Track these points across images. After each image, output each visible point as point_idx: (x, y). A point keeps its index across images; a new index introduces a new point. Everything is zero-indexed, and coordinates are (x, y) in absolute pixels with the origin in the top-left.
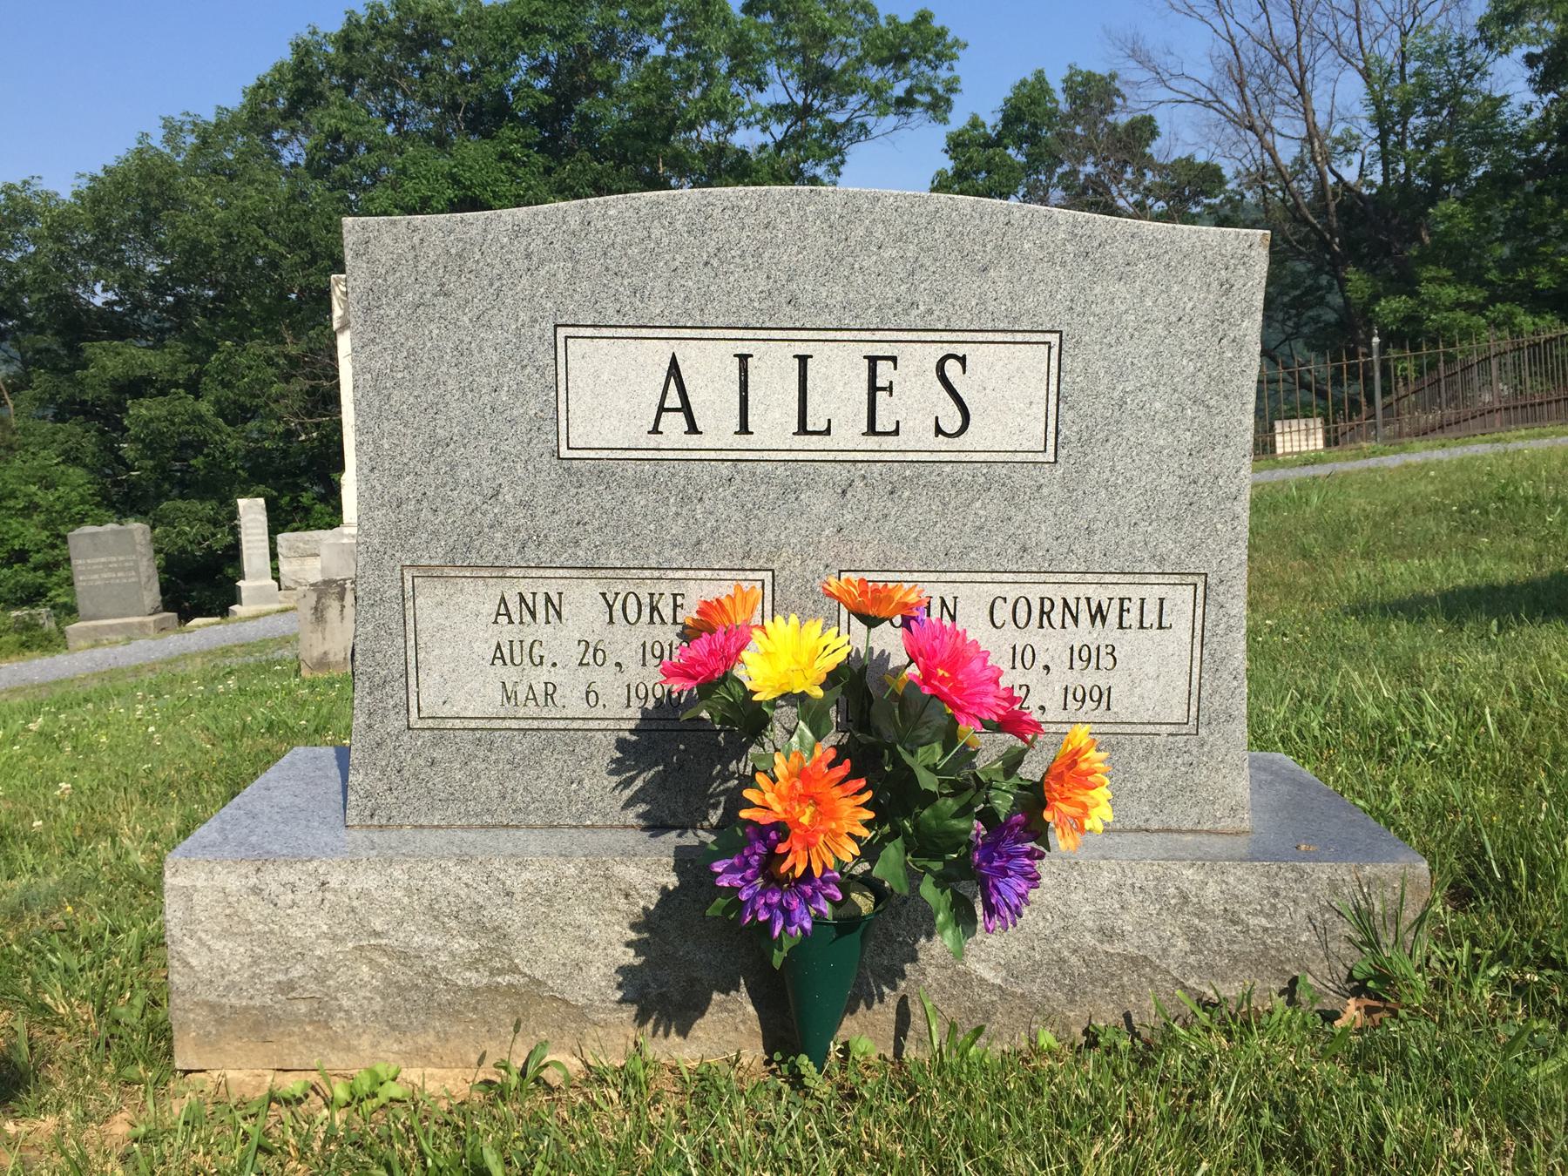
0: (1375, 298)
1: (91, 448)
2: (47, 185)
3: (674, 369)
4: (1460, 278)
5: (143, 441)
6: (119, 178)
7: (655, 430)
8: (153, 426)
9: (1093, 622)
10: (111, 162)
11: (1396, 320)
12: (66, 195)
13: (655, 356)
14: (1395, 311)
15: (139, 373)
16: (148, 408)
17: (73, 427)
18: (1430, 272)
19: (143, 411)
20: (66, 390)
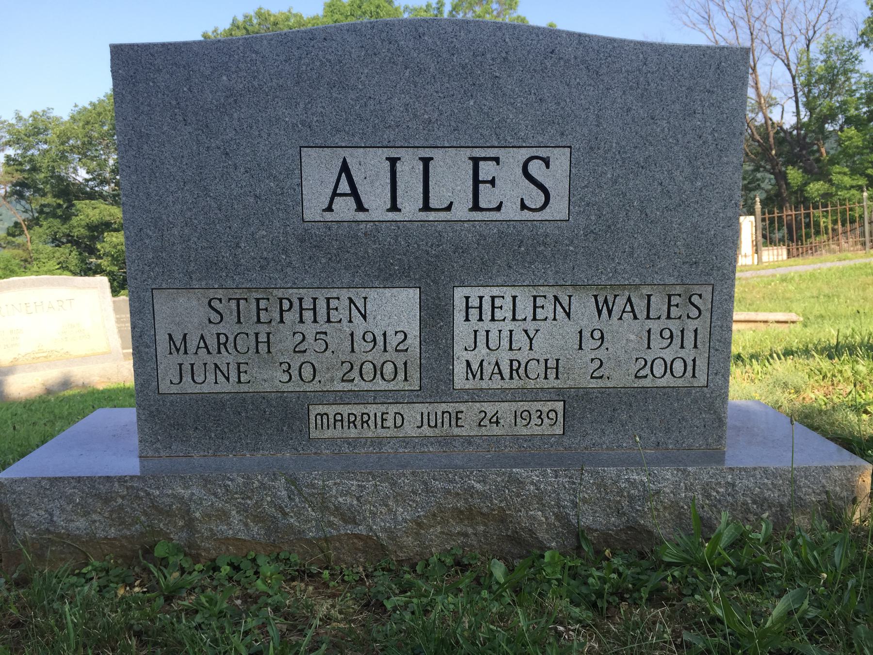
0: (806, 184)
1: (75, 262)
2: (55, 113)
3: (345, 168)
4: (854, 172)
5: (113, 256)
6: (99, 109)
7: (329, 209)
8: (119, 247)
9: (600, 312)
10: (95, 100)
11: (819, 195)
12: (66, 118)
13: (331, 160)
14: (818, 190)
15: (108, 218)
16: (117, 237)
17: (65, 250)
18: (837, 168)
19: (114, 239)
20: (64, 229)
